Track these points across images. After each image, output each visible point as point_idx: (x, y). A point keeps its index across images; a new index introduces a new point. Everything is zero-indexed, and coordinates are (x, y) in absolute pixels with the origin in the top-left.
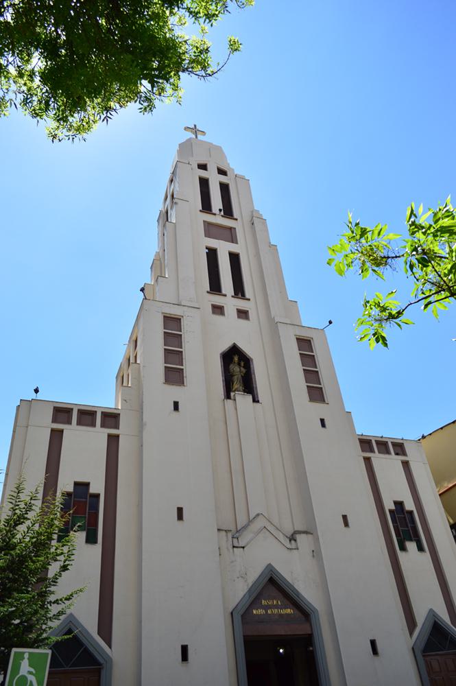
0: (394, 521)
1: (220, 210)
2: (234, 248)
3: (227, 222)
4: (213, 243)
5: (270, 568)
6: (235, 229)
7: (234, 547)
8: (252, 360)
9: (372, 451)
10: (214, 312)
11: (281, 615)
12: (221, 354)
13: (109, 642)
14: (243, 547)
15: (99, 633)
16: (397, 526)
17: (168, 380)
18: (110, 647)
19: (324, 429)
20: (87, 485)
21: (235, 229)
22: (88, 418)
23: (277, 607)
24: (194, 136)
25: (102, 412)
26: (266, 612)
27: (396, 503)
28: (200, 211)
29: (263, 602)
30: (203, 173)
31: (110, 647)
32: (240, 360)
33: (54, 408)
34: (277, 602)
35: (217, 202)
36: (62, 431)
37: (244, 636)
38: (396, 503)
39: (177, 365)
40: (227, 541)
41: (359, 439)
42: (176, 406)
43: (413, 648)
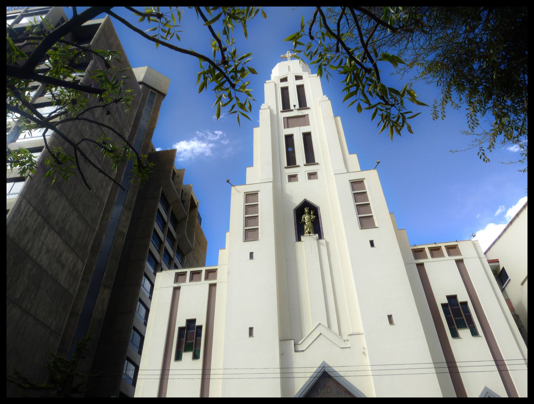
1: (295, 106)
2: (306, 129)
12: (294, 210)
17: (362, 227)
19: (373, 248)
20: (194, 321)
27: (449, 298)
35: (294, 99)
38: (449, 298)
42: (372, 243)
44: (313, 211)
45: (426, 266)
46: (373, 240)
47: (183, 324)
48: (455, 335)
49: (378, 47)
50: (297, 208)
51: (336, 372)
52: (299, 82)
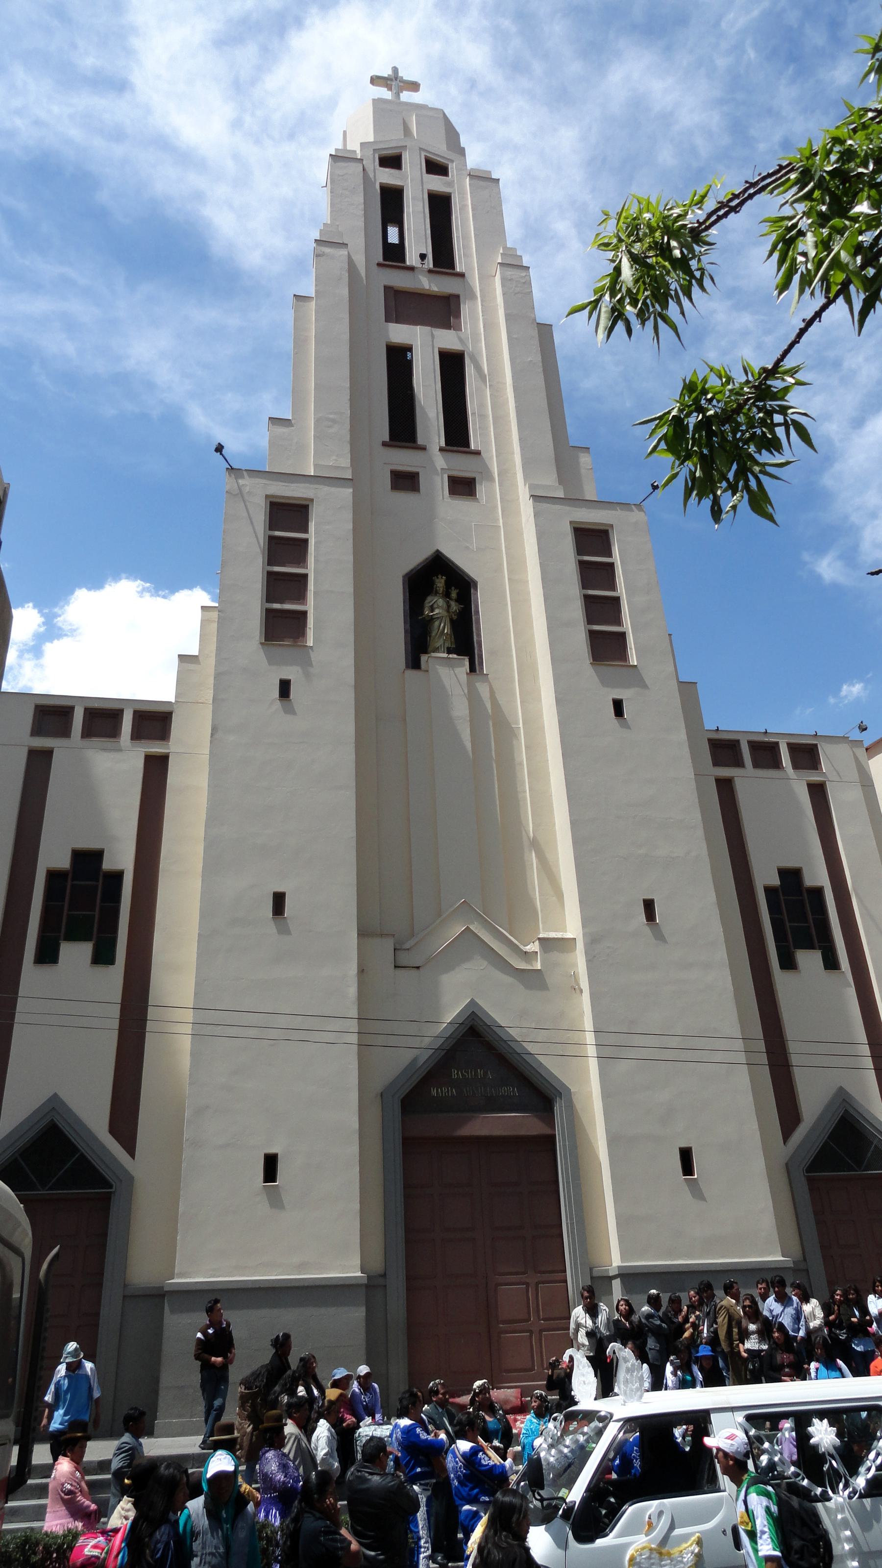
1: (423, 257)
2: (447, 339)
9: (738, 763)
12: (404, 577)
13: (130, 1148)
18: (132, 1154)
20: (98, 855)
27: (783, 873)
28: (379, 265)
31: (132, 1154)
32: (448, 585)
34: (485, 1073)
38: (783, 873)
41: (710, 740)
43: (787, 1164)
44: (456, 588)
47: (64, 862)
49: (865, 127)
50: (414, 572)
51: (502, 1027)
52: (436, 183)
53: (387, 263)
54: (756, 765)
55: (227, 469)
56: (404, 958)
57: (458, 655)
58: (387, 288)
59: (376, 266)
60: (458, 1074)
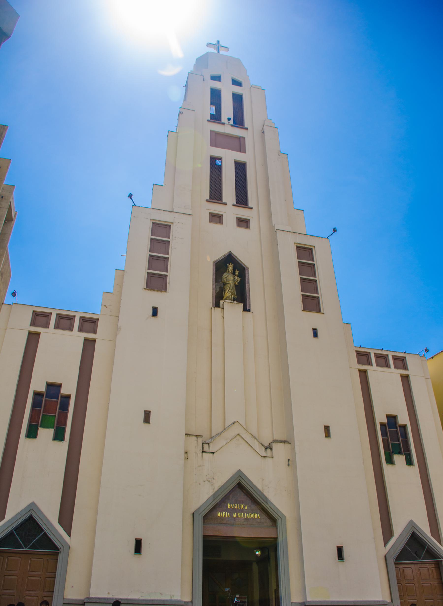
0: (384, 434)
1: (229, 119)
2: (240, 157)
3: (237, 132)
4: (218, 152)
5: (239, 474)
6: (244, 138)
7: (203, 452)
8: (248, 269)
9: (369, 363)
10: (211, 221)
11: (247, 519)
12: (214, 262)
14: (213, 453)
15: (60, 522)
16: (388, 440)
18: (70, 535)
19: (315, 339)
20: (59, 386)
21: (244, 138)
22: (67, 322)
23: (242, 511)
24: (215, 51)
25: (81, 317)
26: (231, 515)
27: (389, 417)
29: (229, 505)
30: (217, 85)
31: (70, 535)
32: (234, 269)
33: (34, 311)
34: (244, 507)
36: (38, 334)
37: (203, 535)
38: (389, 417)
39: (160, 271)
40: (197, 446)
41: (356, 351)
42: (155, 312)
43: (385, 557)
45: (369, 373)
46: (157, 308)
48: (390, 461)
53: (212, 120)
54: (378, 365)
55: (133, 205)
56: (206, 448)
57: (238, 302)
58: (211, 131)
59: (207, 122)
60: (231, 506)
